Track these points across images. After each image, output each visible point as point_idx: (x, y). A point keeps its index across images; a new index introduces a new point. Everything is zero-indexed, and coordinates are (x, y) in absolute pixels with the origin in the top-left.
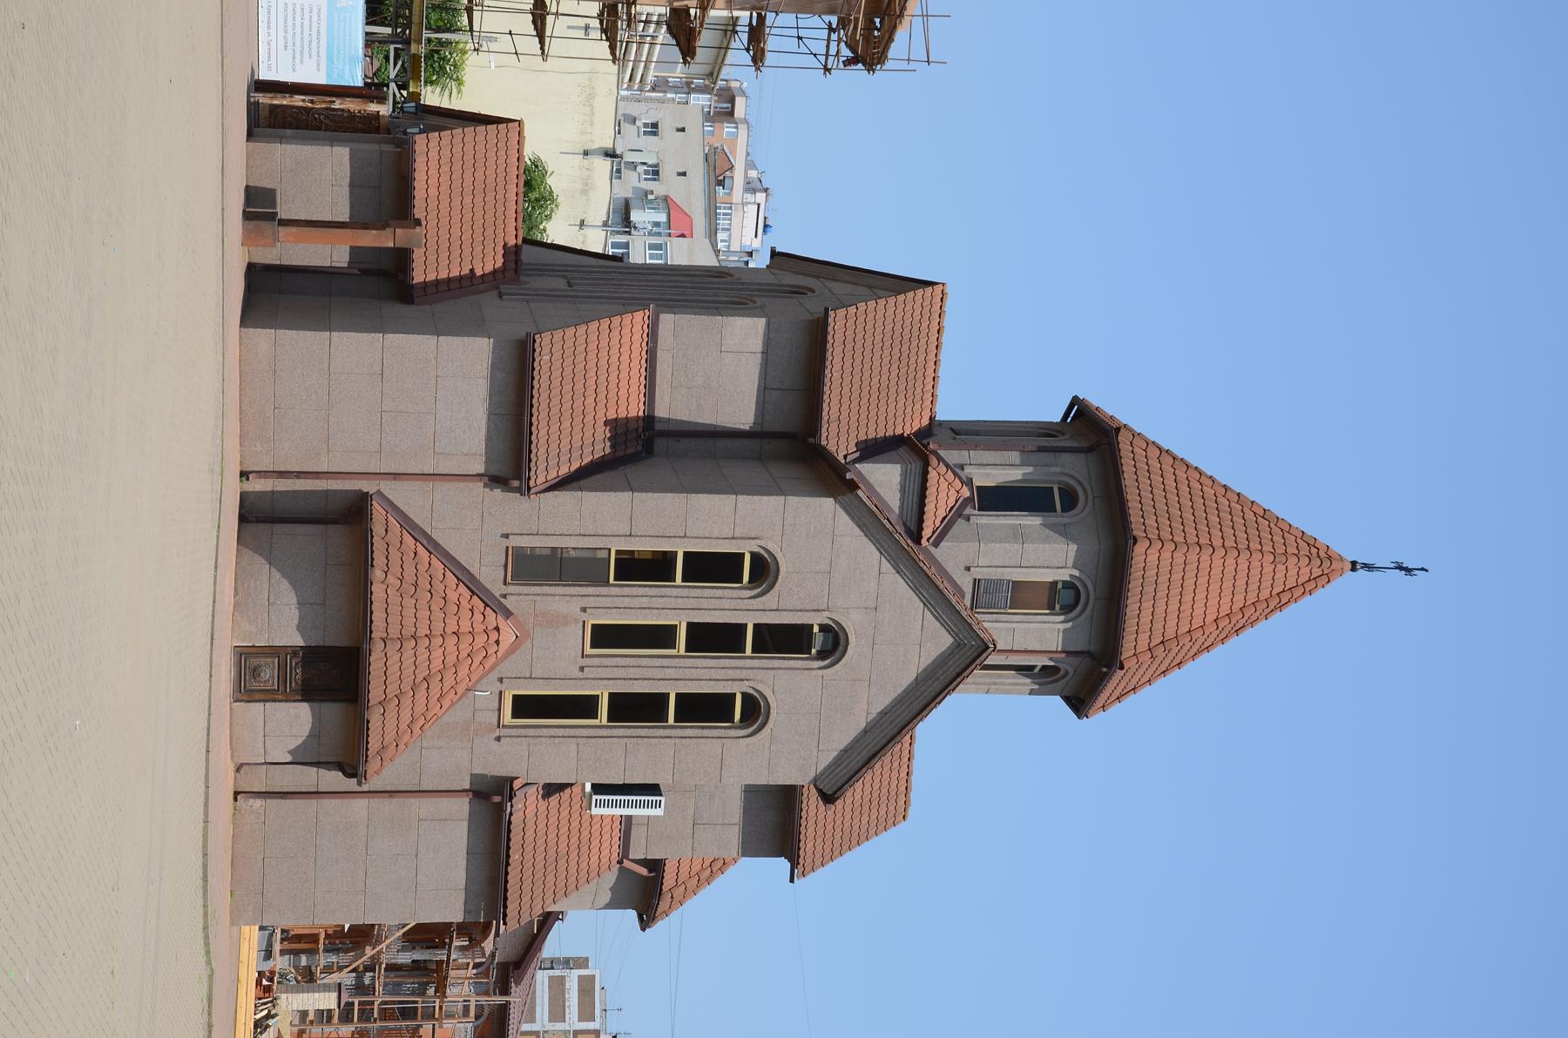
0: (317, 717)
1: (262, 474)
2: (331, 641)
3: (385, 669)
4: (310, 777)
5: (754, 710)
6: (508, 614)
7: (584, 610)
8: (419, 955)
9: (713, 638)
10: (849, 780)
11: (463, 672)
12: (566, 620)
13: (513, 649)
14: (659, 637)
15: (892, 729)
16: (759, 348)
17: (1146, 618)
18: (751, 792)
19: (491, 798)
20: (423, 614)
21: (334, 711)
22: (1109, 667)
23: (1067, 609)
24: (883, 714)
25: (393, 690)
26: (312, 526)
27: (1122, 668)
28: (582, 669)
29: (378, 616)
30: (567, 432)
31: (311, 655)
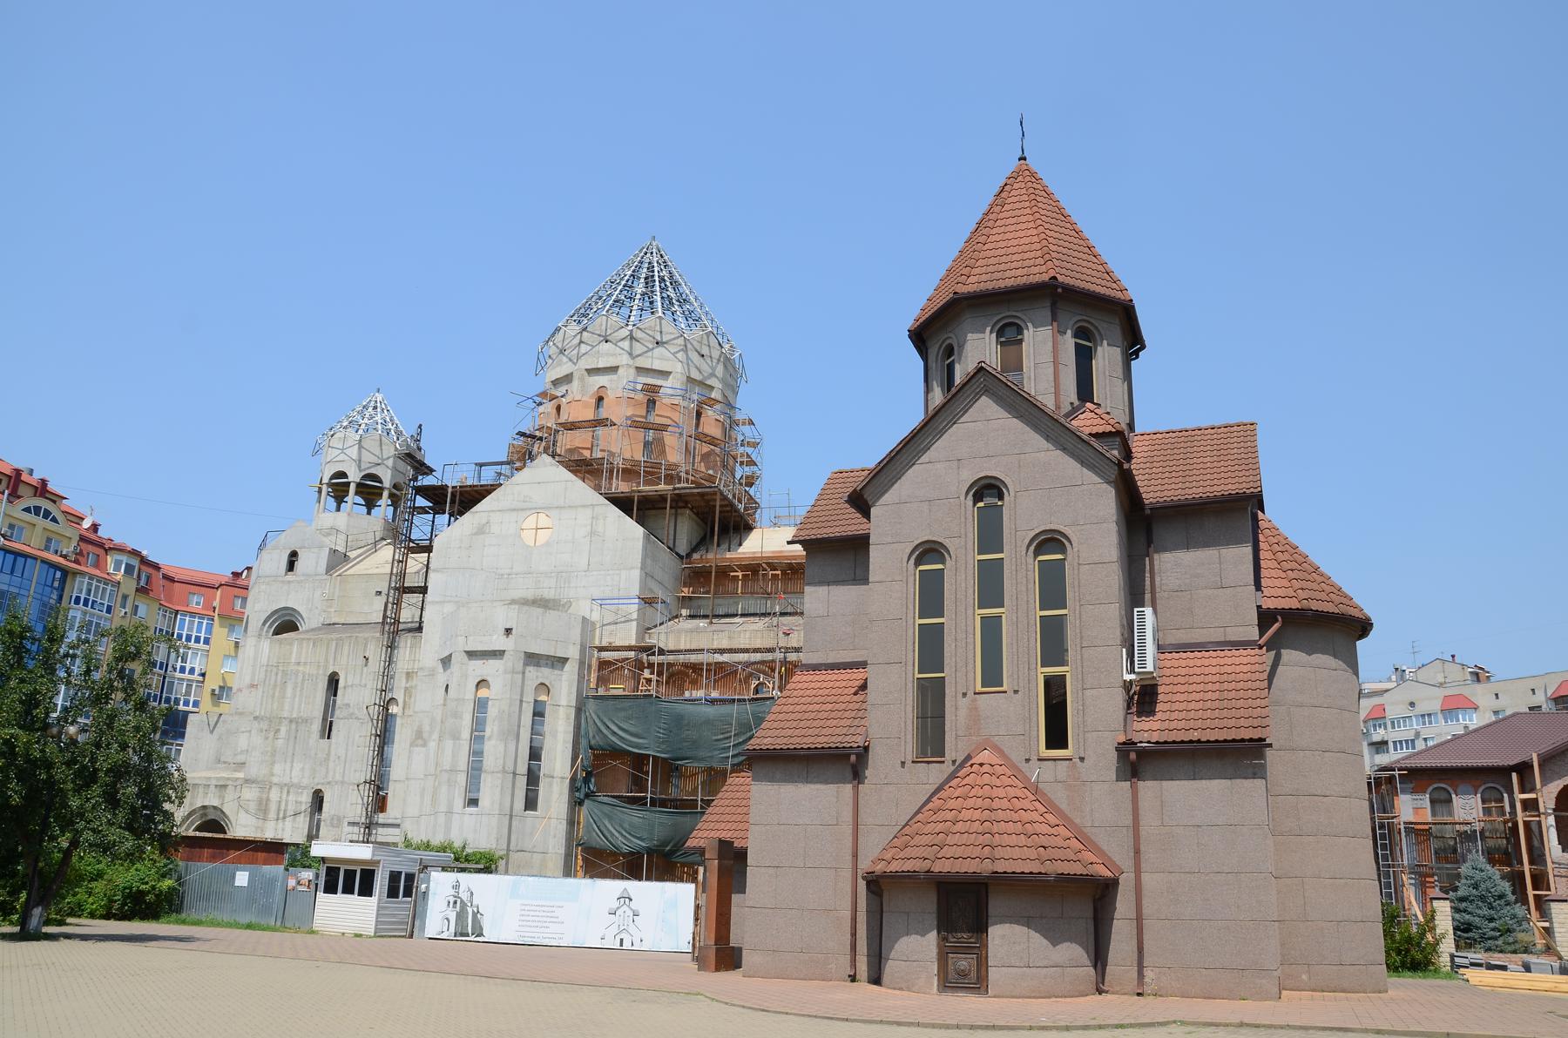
0: (1004, 919)
3: (961, 857)
5: (1050, 541)
6: (969, 757)
7: (964, 695)
9: (990, 587)
12: (974, 709)
14: (992, 629)
16: (826, 588)
19: (1137, 762)
21: (995, 905)
22: (1056, 287)
23: (1020, 330)
24: (1048, 438)
27: (1054, 278)
28: (1016, 692)
31: (946, 925)
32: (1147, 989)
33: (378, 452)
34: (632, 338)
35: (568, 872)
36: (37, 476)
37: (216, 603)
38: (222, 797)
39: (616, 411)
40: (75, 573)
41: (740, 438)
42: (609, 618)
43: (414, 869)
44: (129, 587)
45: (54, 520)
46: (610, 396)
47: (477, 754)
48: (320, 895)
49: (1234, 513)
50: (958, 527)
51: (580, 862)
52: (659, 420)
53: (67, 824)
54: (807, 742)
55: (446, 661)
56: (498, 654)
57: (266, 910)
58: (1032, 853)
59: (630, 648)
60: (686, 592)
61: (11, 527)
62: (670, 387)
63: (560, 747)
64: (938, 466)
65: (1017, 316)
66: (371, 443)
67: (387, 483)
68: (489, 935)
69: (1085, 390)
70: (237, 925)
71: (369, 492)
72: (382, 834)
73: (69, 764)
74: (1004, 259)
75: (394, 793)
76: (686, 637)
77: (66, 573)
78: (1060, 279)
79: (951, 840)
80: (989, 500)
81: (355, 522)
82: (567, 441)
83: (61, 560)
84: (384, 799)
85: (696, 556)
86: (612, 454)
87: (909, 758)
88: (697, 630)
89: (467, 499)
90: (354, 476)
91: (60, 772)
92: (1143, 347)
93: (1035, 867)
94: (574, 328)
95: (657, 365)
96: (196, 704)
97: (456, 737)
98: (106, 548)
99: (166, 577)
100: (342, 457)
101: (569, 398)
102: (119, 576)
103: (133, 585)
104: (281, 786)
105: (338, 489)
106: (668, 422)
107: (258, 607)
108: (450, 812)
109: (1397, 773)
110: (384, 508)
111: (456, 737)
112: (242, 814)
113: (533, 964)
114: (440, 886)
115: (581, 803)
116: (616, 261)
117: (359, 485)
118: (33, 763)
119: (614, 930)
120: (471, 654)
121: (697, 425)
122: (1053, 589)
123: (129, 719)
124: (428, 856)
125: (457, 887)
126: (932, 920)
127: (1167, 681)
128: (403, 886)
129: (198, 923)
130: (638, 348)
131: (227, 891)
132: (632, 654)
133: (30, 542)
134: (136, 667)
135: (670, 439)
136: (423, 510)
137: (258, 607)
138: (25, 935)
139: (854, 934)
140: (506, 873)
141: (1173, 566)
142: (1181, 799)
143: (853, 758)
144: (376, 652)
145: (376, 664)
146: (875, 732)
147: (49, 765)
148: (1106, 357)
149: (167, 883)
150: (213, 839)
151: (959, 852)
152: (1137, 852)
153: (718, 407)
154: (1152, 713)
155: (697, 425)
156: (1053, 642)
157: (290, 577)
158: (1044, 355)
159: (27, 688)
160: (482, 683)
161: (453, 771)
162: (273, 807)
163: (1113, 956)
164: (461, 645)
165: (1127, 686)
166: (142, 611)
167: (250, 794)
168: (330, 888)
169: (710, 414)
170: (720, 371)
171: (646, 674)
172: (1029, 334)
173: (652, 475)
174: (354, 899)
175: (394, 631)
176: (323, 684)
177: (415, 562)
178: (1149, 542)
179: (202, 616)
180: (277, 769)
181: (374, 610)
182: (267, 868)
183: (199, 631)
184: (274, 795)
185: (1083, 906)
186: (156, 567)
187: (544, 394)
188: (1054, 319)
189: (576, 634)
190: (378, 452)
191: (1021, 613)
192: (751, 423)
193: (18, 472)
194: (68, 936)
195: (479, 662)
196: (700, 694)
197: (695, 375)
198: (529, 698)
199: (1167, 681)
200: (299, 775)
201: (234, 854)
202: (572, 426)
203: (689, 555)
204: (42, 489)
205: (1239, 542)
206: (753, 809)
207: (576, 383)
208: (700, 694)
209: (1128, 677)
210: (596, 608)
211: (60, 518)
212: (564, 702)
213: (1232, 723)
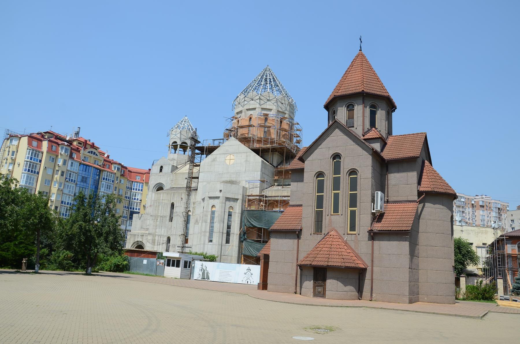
2: (312, 274)
5: (353, 172)
6: (328, 233)
9: (336, 184)
12: (330, 220)
13: (337, 232)
14: (336, 196)
19: (374, 236)
21: (329, 274)
24: (354, 141)
31: (316, 279)
32: (373, 299)
34: (260, 99)
35: (239, 262)
36: (91, 142)
37: (144, 179)
38: (142, 238)
39: (254, 122)
40: (103, 171)
41: (295, 129)
42: (251, 186)
43: (191, 260)
44: (118, 174)
45: (96, 155)
46: (253, 117)
47: (212, 227)
48: (166, 267)
49: (419, 160)
50: (328, 168)
51: (243, 259)
53: (96, 246)
55: (203, 200)
56: (218, 198)
57: (151, 270)
58: (340, 260)
59: (257, 196)
60: (276, 178)
61: (85, 157)
62: (272, 114)
63: (236, 225)
64: (324, 149)
66: (184, 133)
67: (189, 145)
68: (211, 279)
69: (373, 124)
70: (143, 275)
71: (184, 147)
72: (187, 250)
73: (96, 231)
74: (350, 84)
75: (190, 238)
76: (275, 192)
77: (100, 170)
78: (365, 90)
79: (318, 256)
80: (337, 160)
81: (181, 157)
82: (241, 131)
83: (99, 167)
84: (187, 239)
85: (279, 167)
86: (254, 135)
87: (313, 233)
88: (278, 190)
89: (210, 150)
90: (179, 143)
91: (93, 233)
92: (396, 108)
94: (243, 96)
95: (268, 107)
96: (139, 209)
97: (206, 222)
98: (111, 163)
99: (129, 171)
100: (175, 137)
101: (241, 118)
102: (115, 171)
103: (120, 174)
104: (159, 236)
105: (175, 146)
107: (152, 183)
108: (204, 244)
109: (505, 237)
110: (189, 152)
111: (206, 222)
112: (148, 243)
113: (223, 287)
114: (198, 265)
115: (242, 242)
116: (256, 75)
117: (180, 145)
118: (87, 231)
119: (246, 278)
121: (281, 126)
122: (354, 185)
123: (110, 219)
124: (195, 256)
125: (202, 265)
126: (312, 277)
127: (388, 212)
128: (187, 265)
129: (133, 274)
130: (262, 102)
131: (141, 265)
132: (258, 197)
133: (90, 162)
134: (111, 206)
135: (272, 130)
136: (198, 154)
137: (152, 183)
138: (87, 274)
139: (296, 281)
140: (220, 262)
141: (394, 178)
143: (297, 232)
144: (184, 196)
145: (184, 200)
146: (304, 225)
147: (90, 231)
148: (381, 114)
149: (125, 262)
150: (139, 250)
151: (320, 259)
153: (287, 119)
154: (381, 221)
155: (281, 126)
156: (353, 201)
157: (161, 174)
159: (85, 211)
161: (205, 232)
162: (156, 242)
164: (207, 195)
165: (373, 214)
166: (122, 181)
167: (150, 238)
168: (168, 265)
169: (285, 122)
170: (288, 108)
171: (262, 203)
172: (355, 107)
173: (266, 141)
175: (190, 190)
176: (170, 206)
177: (196, 169)
178: (387, 170)
179: (140, 183)
180: (157, 230)
181: (184, 184)
182: (151, 259)
183: (139, 187)
184: (157, 238)
186: (126, 168)
187: (233, 117)
188: (363, 103)
189: (241, 191)
190: (186, 135)
191: (344, 192)
192: (298, 124)
193: (86, 141)
194: (97, 275)
195: (212, 200)
196: (278, 209)
197: (280, 110)
198: (227, 211)
199: (388, 212)
200: (163, 232)
201: (143, 255)
202: (242, 127)
203: (277, 167)
204: (93, 146)
205: (413, 170)
206: (271, 246)
207: (243, 113)
208: (278, 209)
209: (373, 211)
210: (248, 184)
211: (98, 154)
212: (237, 212)
213: (401, 225)
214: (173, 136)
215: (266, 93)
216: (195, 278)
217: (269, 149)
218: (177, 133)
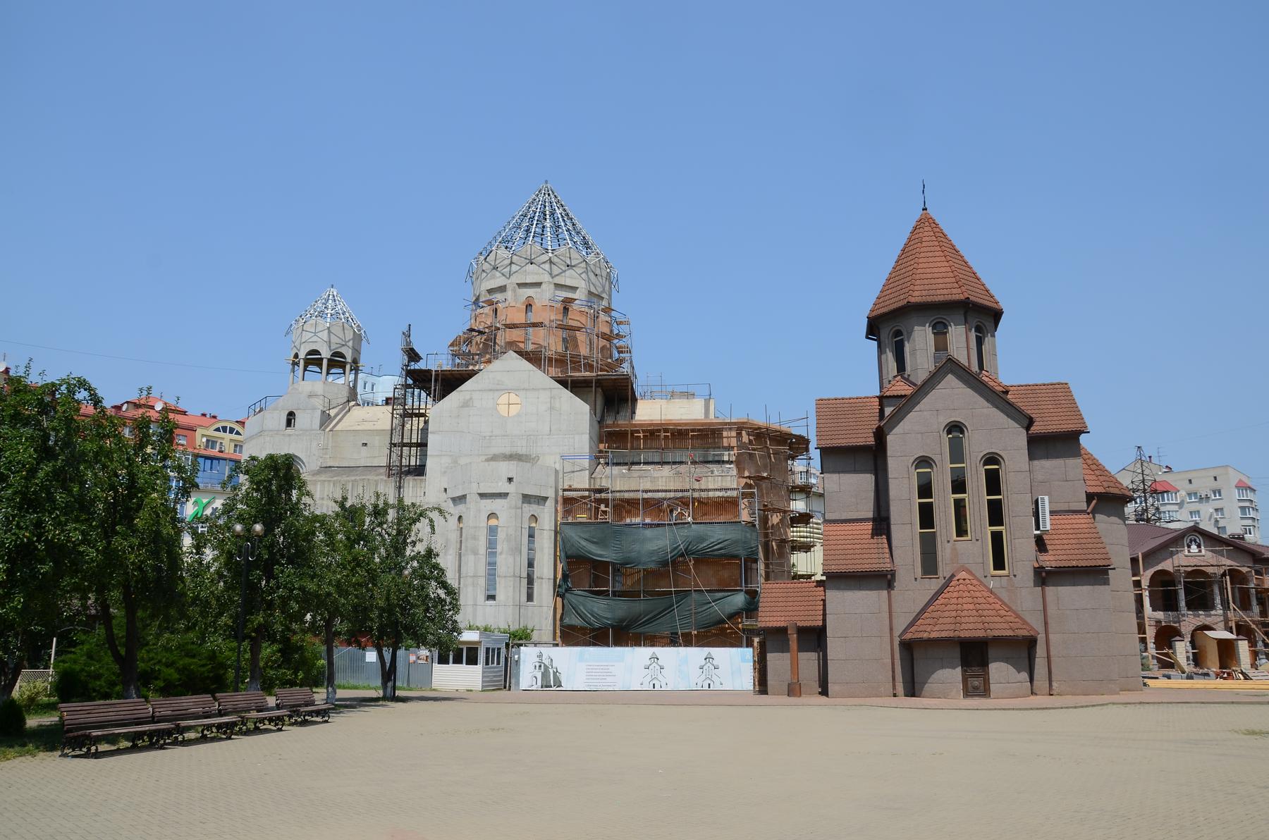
1: (894, 687)
3: (971, 629)
4: (1040, 663)
5: (992, 459)
6: (953, 576)
8: (1254, 602)
9: (959, 485)
10: (1020, 412)
11: (978, 594)
13: (970, 573)
14: (960, 506)
15: (999, 398)
17: (945, 292)
18: (1032, 457)
19: (1044, 577)
20: (947, 614)
21: (992, 652)
23: (946, 326)
24: (988, 401)
25: (980, 626)
26: (915, 662)
29: (944, 634)
30: (871, 557)
31: (966, 663)
33: (341, 335)
34: (551, 262)
42: (568, 468)
46: (537, 304)
47: (492, 564)
50: (939, 449)
52: (572, 323)
54: (859, 568)
65: (936, 314)
67: (349, 359)
68: (565, 686)
76: (622, 480)
78: (972, 298)
93: (951, 634)
100: (315, 339)
106: (579, 325)
111: (475, 553)
117: (329, 360)
120: (482, 495)
125: (540, 656)
130: (556, 270)
132: (587, 493)
135: (581, 337)
139: (893, 672)
142: (1066, 596)
152: (1046, 623)
157: (289, 431)
158: (959, 339)
160: (492, 515)
163: (1036, 676)
168: (443, 660)
174: (463, 667)
185: (1023, 650)
190: (341, 335)
191: (977, 497)
196: (637, 520)
197: (593, 290)
208: (637, 520)
212: (547, 527)
214: (306, 336)
215: (563, 249)
216: (523, 685)
217: (591, 381)
218: (319, 329)
